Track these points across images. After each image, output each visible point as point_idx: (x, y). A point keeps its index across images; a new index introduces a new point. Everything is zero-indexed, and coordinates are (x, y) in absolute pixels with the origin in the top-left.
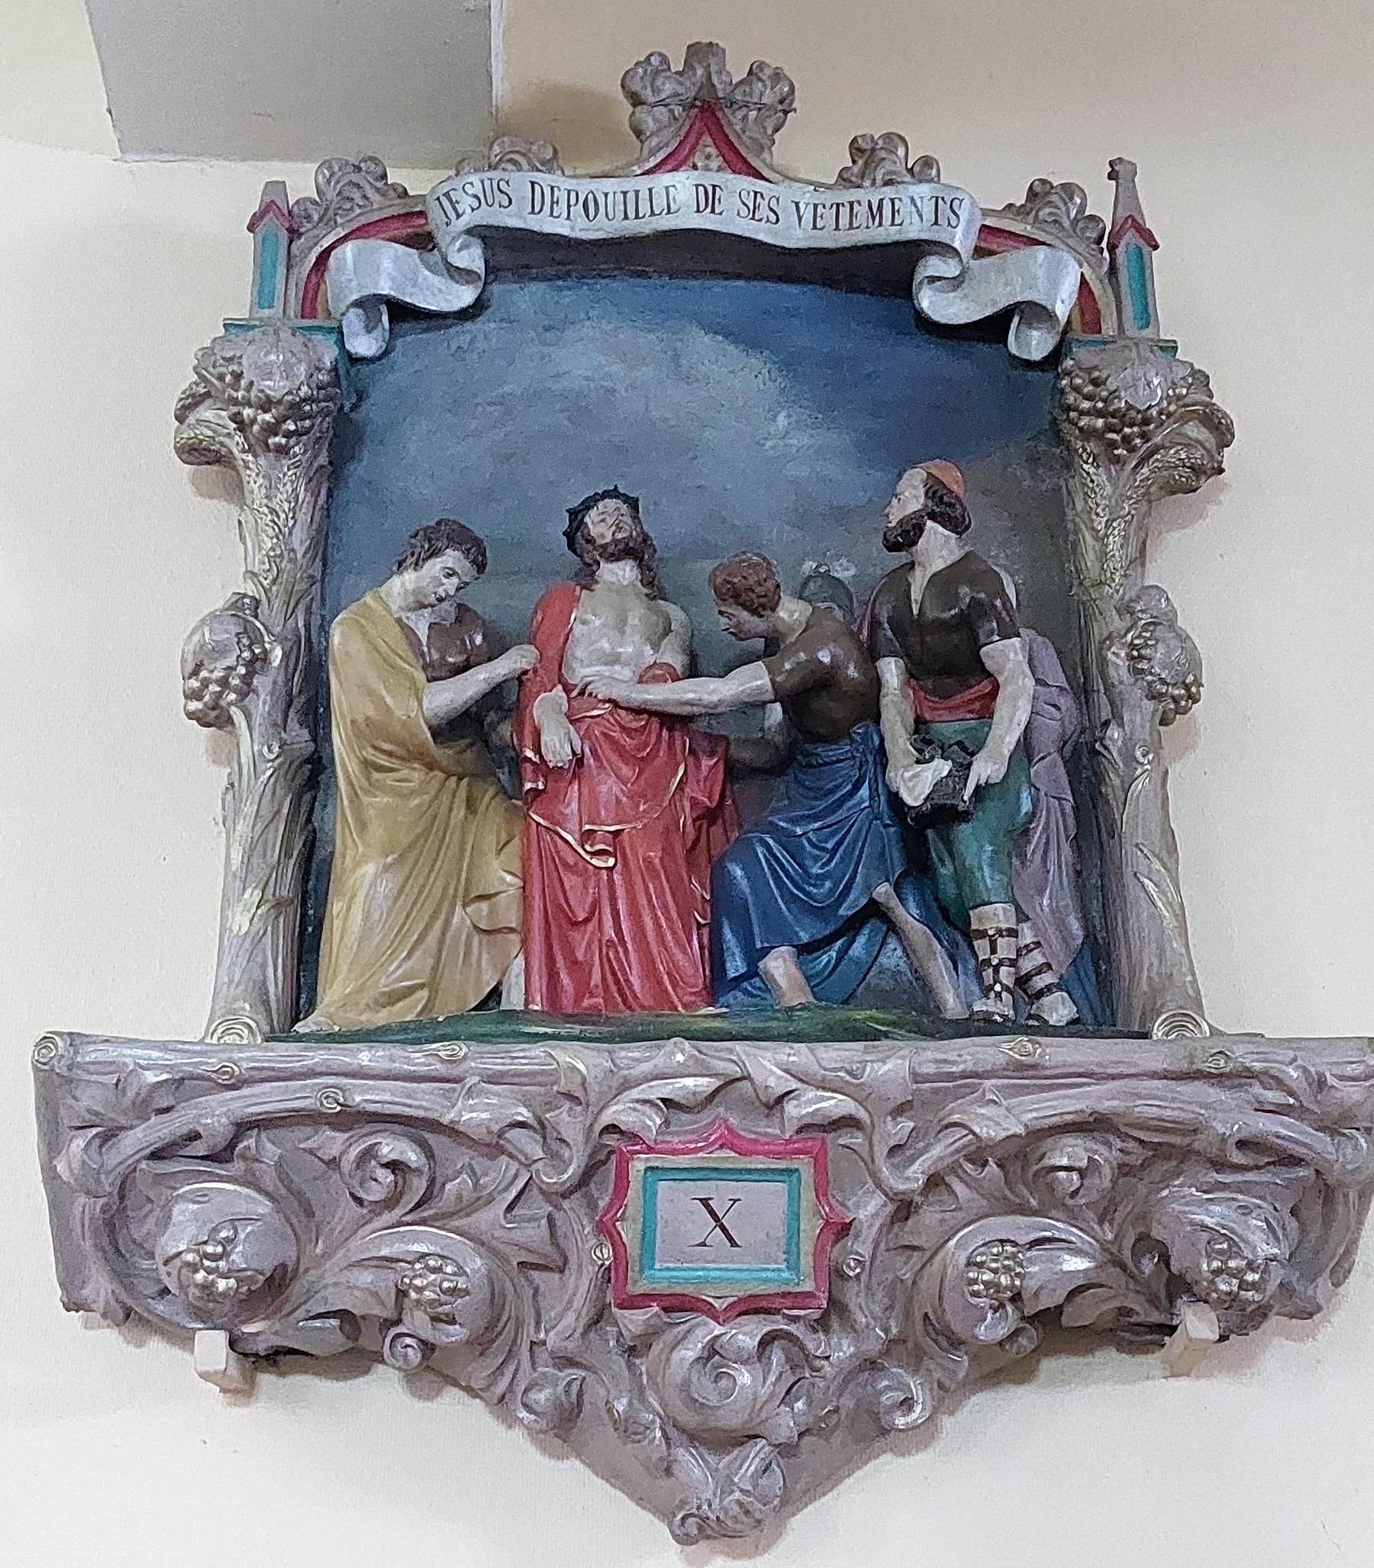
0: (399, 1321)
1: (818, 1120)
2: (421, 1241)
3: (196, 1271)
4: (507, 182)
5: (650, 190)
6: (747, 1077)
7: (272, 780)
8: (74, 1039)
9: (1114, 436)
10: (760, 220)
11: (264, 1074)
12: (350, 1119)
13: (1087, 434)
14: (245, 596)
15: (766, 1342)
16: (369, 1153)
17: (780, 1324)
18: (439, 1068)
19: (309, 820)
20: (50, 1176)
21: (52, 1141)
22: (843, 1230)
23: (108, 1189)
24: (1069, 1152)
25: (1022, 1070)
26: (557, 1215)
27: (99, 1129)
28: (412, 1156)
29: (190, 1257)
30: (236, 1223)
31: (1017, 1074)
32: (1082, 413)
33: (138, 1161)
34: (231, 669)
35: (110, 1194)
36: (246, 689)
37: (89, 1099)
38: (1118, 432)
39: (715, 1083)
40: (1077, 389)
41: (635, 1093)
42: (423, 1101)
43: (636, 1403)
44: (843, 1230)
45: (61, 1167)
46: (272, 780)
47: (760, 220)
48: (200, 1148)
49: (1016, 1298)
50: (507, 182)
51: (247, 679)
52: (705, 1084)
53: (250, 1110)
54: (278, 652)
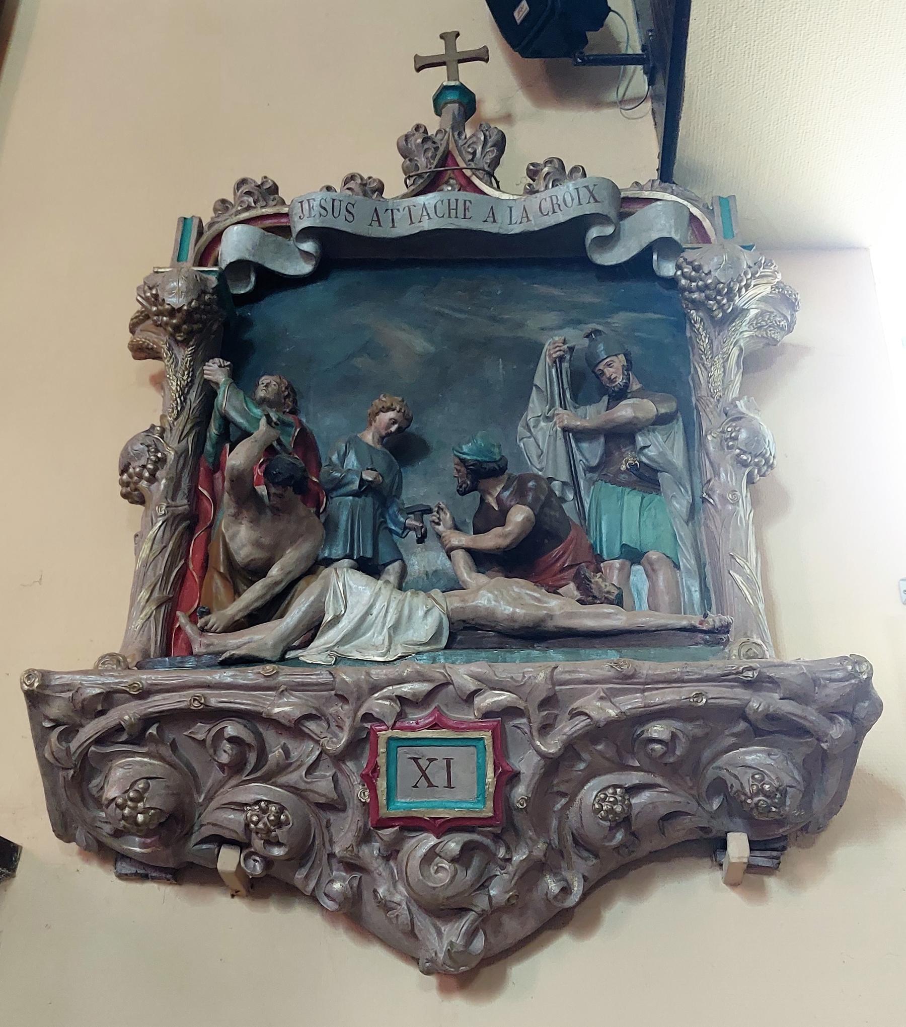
1: (495, 708)
2: (255, 791)
4: (353, 205)
5: (449, 200)
7: (162, 528)
15: (468, 849)
21: (40, 740)
22: (514, 777)
25: (626, 679)
26: (339, 775)
27: (62, 728)
29: (120, 801)
30: (149, 781)
32: (691, 292)
34: (144, 467)
36: (153, 479)
37: (56, 709)
42: (243, 701)
44: (514, 777)
46: (162, 528)
48: (124, 737)
50: (353, 205)
51: (153, 474)
53: (150, 710)
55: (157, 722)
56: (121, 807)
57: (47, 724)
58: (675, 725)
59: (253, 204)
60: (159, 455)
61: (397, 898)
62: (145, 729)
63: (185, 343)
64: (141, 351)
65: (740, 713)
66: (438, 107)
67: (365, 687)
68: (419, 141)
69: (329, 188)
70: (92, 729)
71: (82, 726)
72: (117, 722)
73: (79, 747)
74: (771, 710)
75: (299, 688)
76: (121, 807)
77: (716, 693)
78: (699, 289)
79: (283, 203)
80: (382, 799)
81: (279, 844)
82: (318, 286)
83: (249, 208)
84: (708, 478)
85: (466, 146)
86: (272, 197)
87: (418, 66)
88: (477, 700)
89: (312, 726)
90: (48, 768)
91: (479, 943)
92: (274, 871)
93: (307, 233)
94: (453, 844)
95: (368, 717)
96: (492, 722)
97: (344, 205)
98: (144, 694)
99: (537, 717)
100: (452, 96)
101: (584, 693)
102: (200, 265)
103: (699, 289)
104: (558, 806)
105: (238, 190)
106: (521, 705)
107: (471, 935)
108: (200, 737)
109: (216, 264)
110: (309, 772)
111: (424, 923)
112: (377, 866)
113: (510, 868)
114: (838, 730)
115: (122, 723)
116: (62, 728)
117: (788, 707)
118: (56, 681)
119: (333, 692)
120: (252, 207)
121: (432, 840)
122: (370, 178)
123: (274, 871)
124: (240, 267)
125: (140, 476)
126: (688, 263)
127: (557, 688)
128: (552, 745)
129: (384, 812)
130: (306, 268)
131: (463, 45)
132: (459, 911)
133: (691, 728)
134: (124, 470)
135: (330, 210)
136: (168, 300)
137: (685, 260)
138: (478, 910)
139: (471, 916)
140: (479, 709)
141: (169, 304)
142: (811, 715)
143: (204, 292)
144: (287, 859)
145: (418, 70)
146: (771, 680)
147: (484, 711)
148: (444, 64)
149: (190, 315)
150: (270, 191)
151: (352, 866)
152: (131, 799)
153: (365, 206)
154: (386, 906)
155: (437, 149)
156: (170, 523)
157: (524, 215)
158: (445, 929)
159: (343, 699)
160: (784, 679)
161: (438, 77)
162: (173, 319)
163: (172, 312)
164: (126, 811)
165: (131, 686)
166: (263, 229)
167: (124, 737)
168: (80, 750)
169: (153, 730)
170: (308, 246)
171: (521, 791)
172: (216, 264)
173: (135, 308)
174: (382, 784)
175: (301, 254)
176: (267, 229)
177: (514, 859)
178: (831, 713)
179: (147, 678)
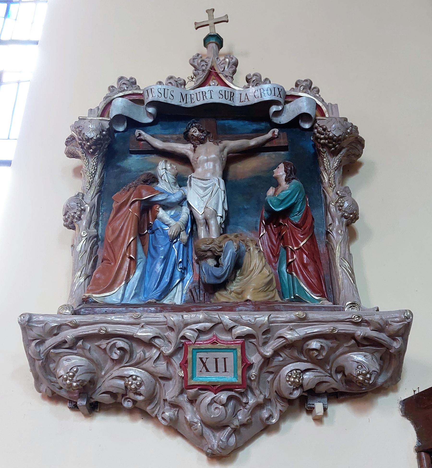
0: (127, 395)
2: (132, 371)
3: (66, 380)
6: (221, 323)
8: (31, 316)
9: (331, 145)
10: (243, 102)
11: (82, 323)
12: (108, 336)
13: (323, 145)
14: (80, 193)
15: (230, 398)
16: (115, 344)
17: (233, 393)
18: (132, 320)
19: (96, 253)
20: (28, 355)
21: (27, 345)
22: (250, 366)
23: (43, 357)
24: (314, 344)
27: (38, 341)
28: (126, 347)
31: (299, 321)
33: (50, 349)
35: (43, 359)
37: (34, 333)
38: (331, 143)
39: (213, 324)
40: (318, 132)
41: (188, 327)
43: (193, 416)
45: (30, 352)
47: (243, 102)
48: (67, 346)
49: (301, 386)
52: (209, 325)
54: (89, 208)
55: (82, 339)
56: (66, 379)
57: (30, 338)
58: (324, 342)
59: (126, 89)
60: (82, 208)
61: (196, 420)
62: (77, 343)
63: (93, 154)
64: (71, 155)
65: (352, 336)
66: (205, 45)
67: (182, 325)
68: (199, 61)
69: (160, 83)
70: (51, 341)
71: (46, 340)
72: (64, 338)
73: (46, 349)
74: (366, 335)
75: (151, 324)
76: (66, 379)
77: (342, 328)
78: (325, 139)
79: (139, 88)
80: (189, 375)
81: (140, 394)
82: (320, 246)
83: (124, 90)
84: (330, 223)
85: (220, 64)
86: (134, 86)
87: (196, 27)
88: (233, 330)
89: (157, 341)
90: (32, 361)
91: (233, 440)
92: (137, 405)
93: (152, 104)
94: (223, 396)
95: (184, 337)
96: (240, 341)
97: (169, 91)
98: (76, 326)
99: (262, 338)
100: (213, 40)
101: (281, 327)
102: (101, 116)
103: (325, 139)
104: (269, 379)
105: (119, 82)
106: (254, 332)
107: (229, 436)
108: (103, 347)
109: (108, 117)
110: (154, 362)
111: (207, 432)
112: (188, 407)
113: (248, 407)
114: (396, 345)
115: (66, 340)
116: (38, 341)
117: (374, 334)
118: (35, 319)
119: (167, 326)
120: (126, 90)
121: (213, 395)
122: (179, 78)
123: (137, 405)
124: (119, 118)
125: (73, 217)
126: (320, 127)
127: (270, 325)
128: (268, 351)
129: (191, 382)
130: (150, 120)
131: (217, 15)
132: (225, 427)
133: (329, 343)
134: (65, 215)
135: (163, 95)
136: (86, 134)
137: (319, 125)
138: (233, 426)
139: (229, 429)
140: (235, 335)
141: (87, 136)
142: (383, 336)
143: (103, 131)
144: (143, 401)
145: (197, 29)
146: (367, 322)
147: (237, 335)
148: (208, 25)
149: (97, 142)
150: (133, 83)
151: (174, 405)
152: (70, 376)
153: (177, 91)
154: (191, 425)
155: (207, 65)
156: (88, 240)
157: (246, 98)
158: (217, 435)
159: (171, 329)
160: (371, 320)
161: (205, 31)
162: (88, 142)
163: (88, 140)
164: (68, 381)
165: (71, 322)
166: (130, 100)
167: (67, 346)
168: (46, 351)
169: (80, 343)
170: (151, 110)
171: (253, 372)
172: (108, 117)
173: (69, 133)
174: (189, 370)
175: (147, 113)
176: (133, 101)
177: (250, 402)
178: (393, 337)
179: (77, 319)
